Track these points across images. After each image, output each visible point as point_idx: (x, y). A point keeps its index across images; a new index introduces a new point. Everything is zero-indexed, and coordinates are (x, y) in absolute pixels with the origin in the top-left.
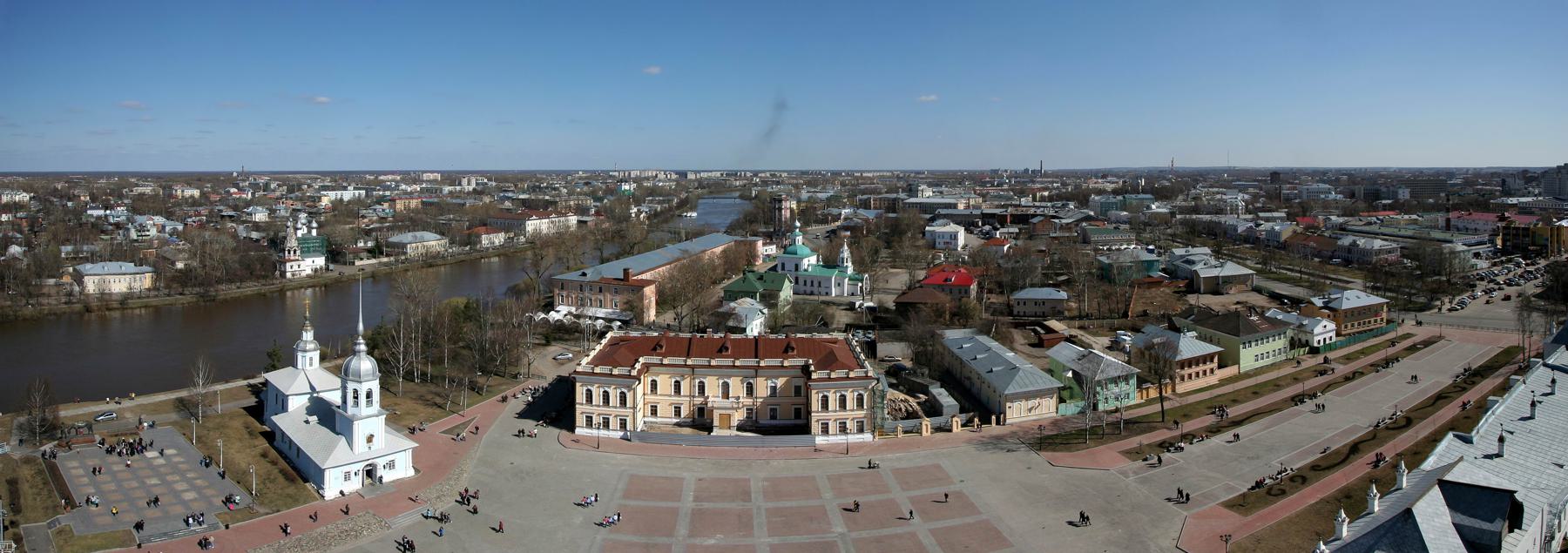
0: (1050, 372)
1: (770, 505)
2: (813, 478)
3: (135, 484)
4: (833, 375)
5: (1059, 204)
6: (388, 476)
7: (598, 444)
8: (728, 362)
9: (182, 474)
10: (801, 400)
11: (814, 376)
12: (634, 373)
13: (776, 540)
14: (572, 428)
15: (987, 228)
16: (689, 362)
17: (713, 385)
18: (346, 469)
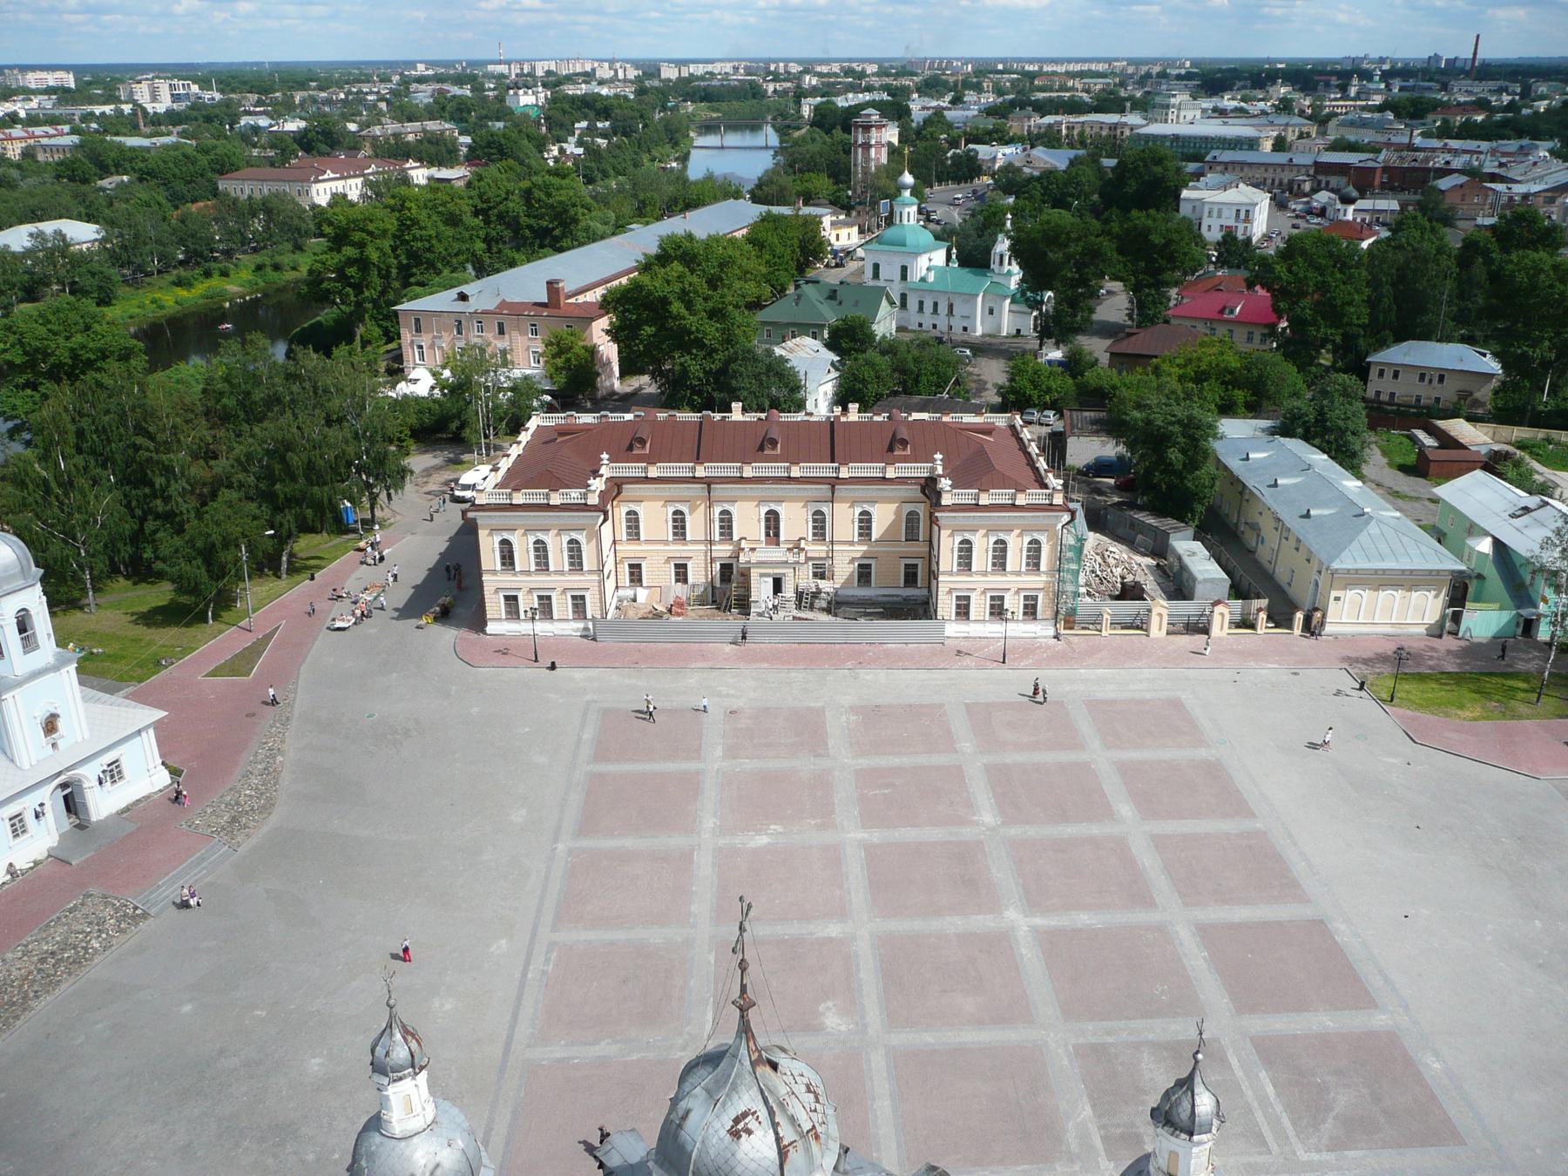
0: (1440, 537)
1: (864, 762)
4: (985, 500)
5: (1512, 145)
7: (534, 653)
8: (776, 469)
10: (920, 548)
11: (946, 500)
12: (593, 500)
13: (876, 836)
14: (478, 621)
16: (700, 472)
17: (748, 519)
18: (12, 809)
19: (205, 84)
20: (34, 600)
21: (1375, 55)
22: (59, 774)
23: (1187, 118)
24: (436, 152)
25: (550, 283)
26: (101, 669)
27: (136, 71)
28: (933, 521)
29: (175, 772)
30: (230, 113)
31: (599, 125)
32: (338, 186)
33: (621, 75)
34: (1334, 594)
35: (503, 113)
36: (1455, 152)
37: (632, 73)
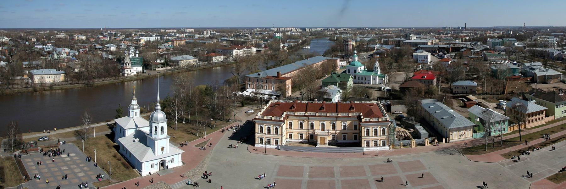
2: (363, 167)
4: (372, 120)
5: (474, 43)
6: (171, 166)
7: (265, 151)
8: (324, 114)
11: (363, 120)
12: (282, 119)
14: (253, 144)
15: (441, 53)
16: (307, 114)
17: (317, 125)
18: (152, 162)
21: (448, 27)
23: (414, 39)
28: (360, 126)
29: (183, 163)
34: (450, 133)
36: (464, 44)
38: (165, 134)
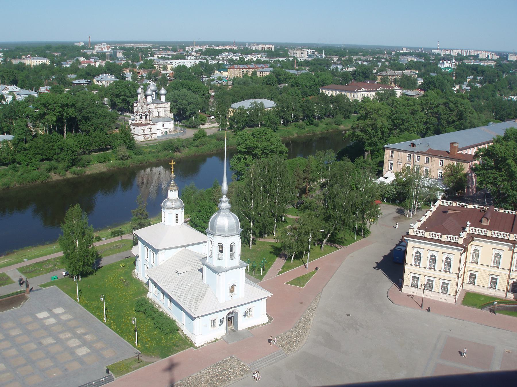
3: (33, 346)
6: (243, 324)
9: (72, 330)
19: (320, 51)
20: (237, 240)
22: (231, 308)
24: (406, 83)
25: (452, 143)
26: (255, 271)
27: (294, 47)
29: (270, 318)
30: (328, 63)
31: (479, 78)
32: (366, 94)
33: (490, 57)
35: (437, 70)
37: (495, 57)
38: (238, 260)
